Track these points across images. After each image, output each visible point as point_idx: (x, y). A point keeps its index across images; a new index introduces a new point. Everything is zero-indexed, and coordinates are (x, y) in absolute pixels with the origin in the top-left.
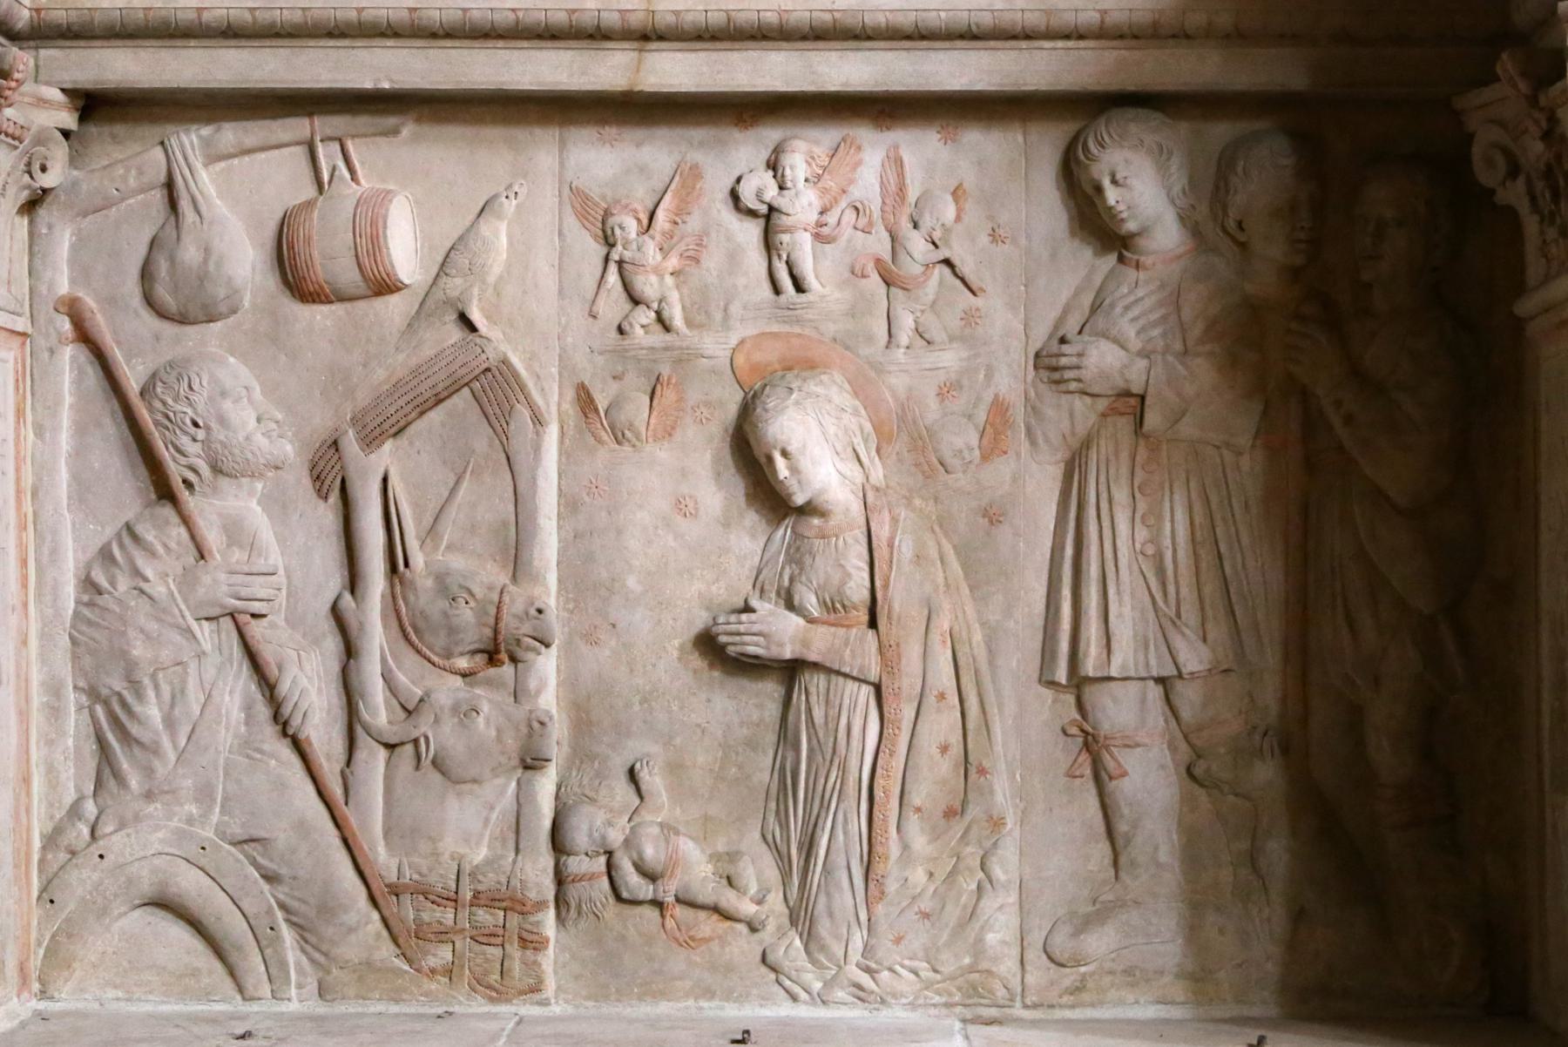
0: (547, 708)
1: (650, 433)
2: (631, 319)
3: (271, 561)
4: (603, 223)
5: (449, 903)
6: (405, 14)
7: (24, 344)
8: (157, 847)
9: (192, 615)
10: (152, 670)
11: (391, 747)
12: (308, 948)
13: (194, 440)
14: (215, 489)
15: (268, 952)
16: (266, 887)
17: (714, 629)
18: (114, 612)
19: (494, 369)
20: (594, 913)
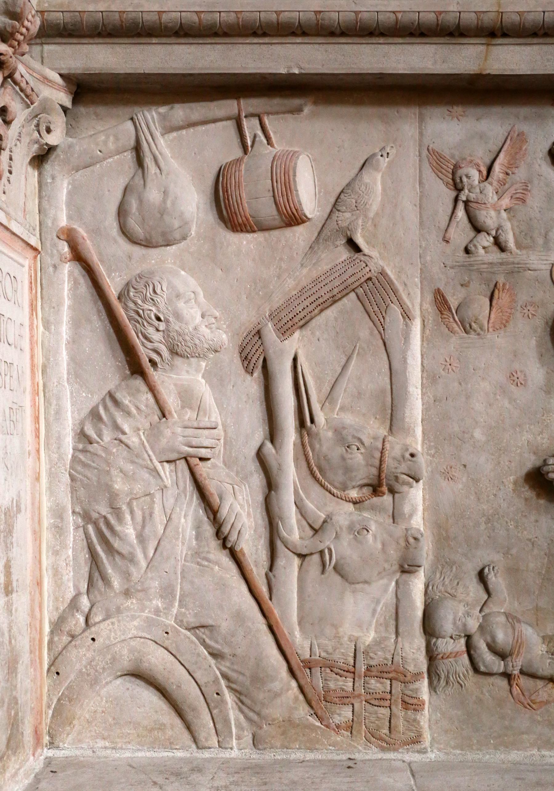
0: (417, 527)
1: (490, 325)
2: (475, 242)
3: (213, 419)
4: (453, 174)
5: (348, 674)
6: (312, 16)
7: (35, 257)
8: (134, 632)
9: (157, 459)
10: (128, 499)
11: (302, 556)
12: (244, 707)
13: (158, 330)
14: (172, 366)
15: (215, 712)
16: (212, 661)
17: (545, 469)
18: (102, 457)
19: (374, 280)
20: (458, 682)
